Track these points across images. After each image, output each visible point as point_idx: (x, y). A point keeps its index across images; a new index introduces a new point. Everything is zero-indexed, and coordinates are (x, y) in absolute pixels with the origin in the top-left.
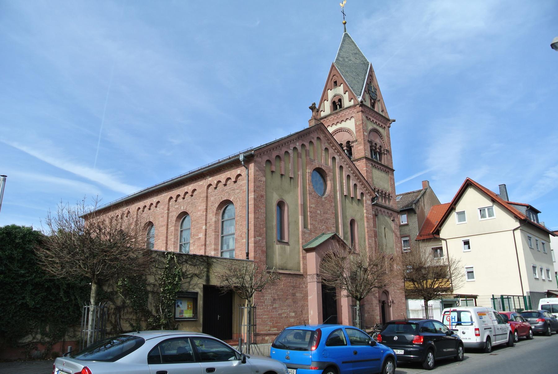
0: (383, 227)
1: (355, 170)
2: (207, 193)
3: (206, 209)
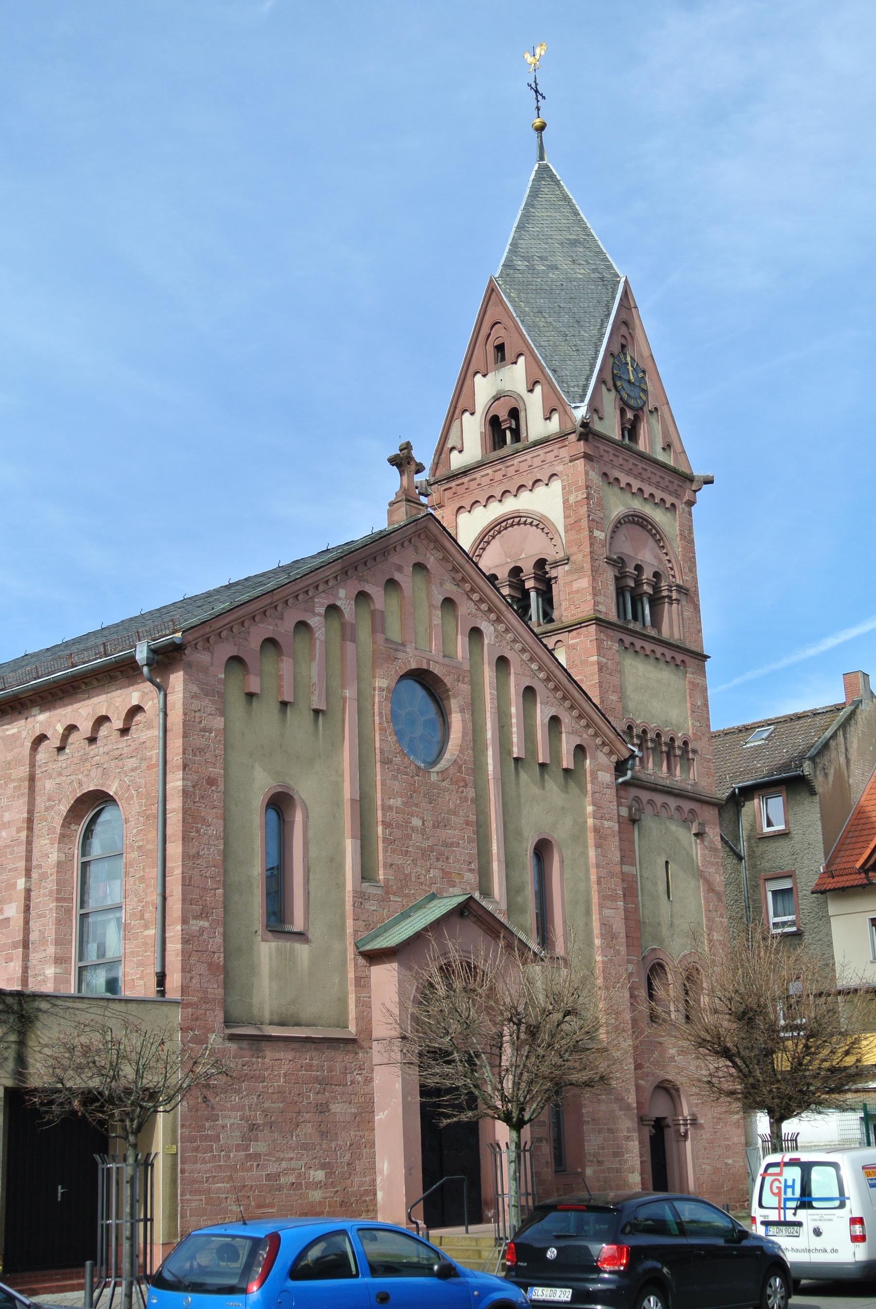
0: (661, 861)
1: (553, 667)
2: (32, 764)
3: (30, 821)
